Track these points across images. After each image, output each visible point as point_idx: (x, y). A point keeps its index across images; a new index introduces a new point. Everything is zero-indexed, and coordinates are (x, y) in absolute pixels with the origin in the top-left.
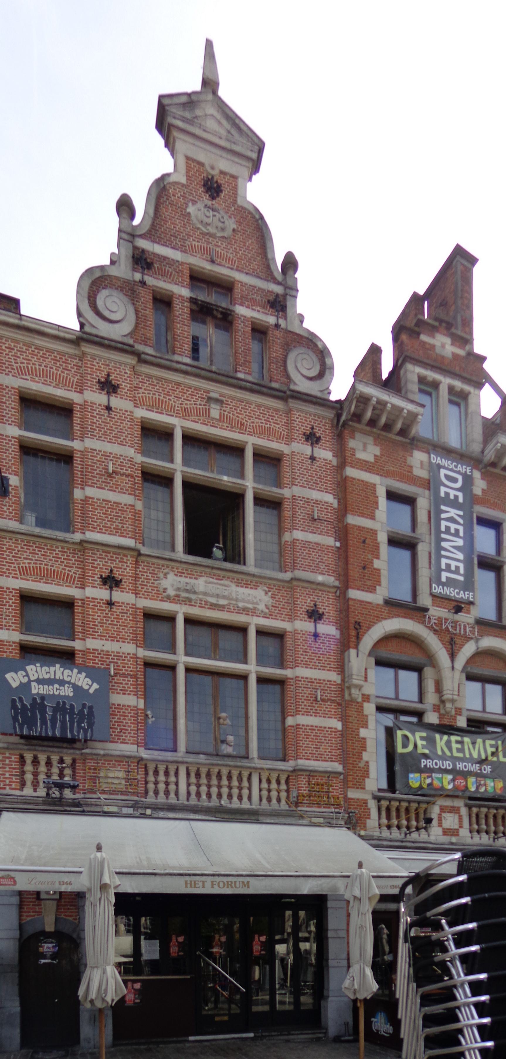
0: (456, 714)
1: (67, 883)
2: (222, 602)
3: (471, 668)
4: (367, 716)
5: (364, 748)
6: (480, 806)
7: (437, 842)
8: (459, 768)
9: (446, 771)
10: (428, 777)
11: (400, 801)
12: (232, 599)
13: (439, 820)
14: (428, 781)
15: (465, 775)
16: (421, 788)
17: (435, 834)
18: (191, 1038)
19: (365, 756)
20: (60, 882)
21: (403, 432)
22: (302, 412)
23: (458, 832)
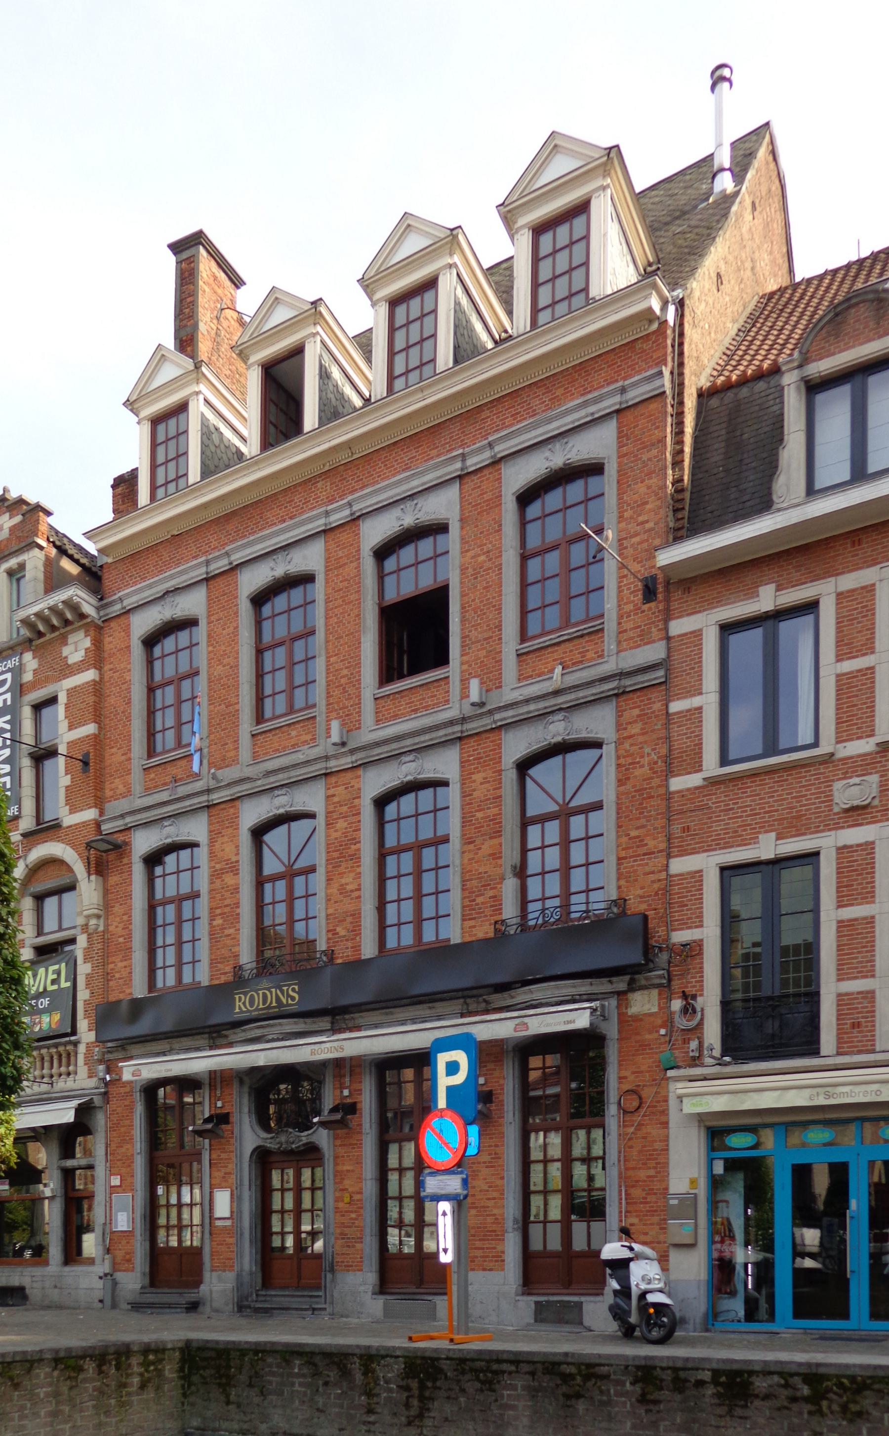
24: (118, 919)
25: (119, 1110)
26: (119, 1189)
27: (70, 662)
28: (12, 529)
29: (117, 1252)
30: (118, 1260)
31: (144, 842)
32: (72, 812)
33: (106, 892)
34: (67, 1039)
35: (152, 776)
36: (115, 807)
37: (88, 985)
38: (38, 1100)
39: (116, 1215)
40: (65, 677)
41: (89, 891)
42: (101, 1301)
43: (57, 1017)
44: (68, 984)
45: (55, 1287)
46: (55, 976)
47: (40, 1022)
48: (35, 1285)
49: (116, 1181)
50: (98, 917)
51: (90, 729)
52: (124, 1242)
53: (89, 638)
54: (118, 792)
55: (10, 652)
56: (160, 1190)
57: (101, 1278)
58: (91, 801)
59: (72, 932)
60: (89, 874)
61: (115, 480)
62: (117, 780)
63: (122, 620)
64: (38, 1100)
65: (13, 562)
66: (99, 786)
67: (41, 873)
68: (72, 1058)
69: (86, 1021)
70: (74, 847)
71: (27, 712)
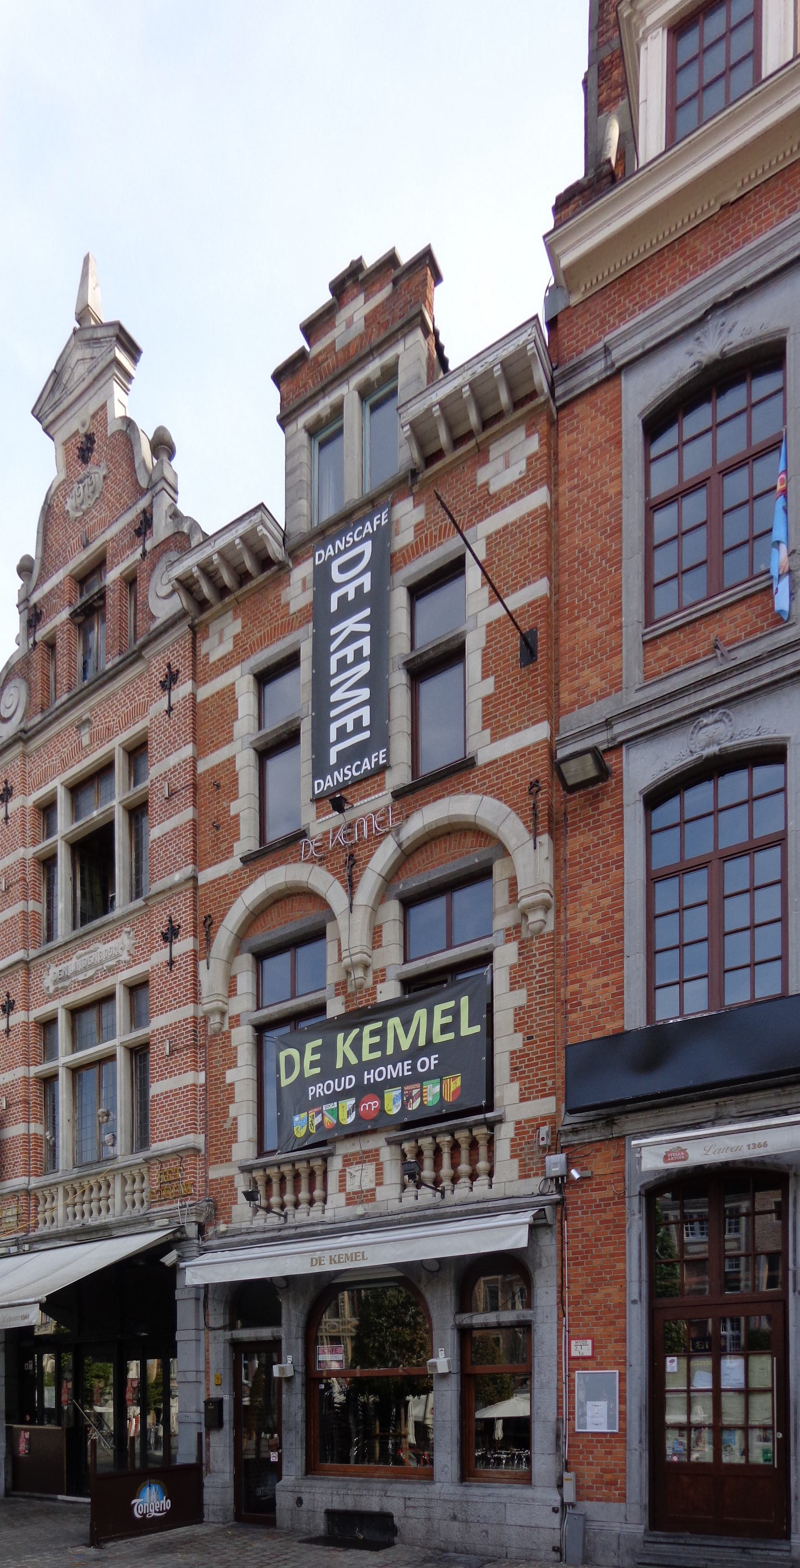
0: (375, 983)
1: (760, 1146)
2: (90, 973)
3: (404, 884)
4: (236, 1048)
5: (231, 1099)
6: (415, 1138)
7: (337, 1219)
8: (369, 1079)
9: (345, 1094)
10: (317, 1114)
11: (278, 1165)
12: (97, 965)
13: (340, 1181)
14: (317, 1120)
15: (378, 1090)
16: (308, 1134)
17: (336, 1207)
18: (60, 1497)
19: (233, 1110)
20: (749, 1146)
21: (265, 562)
22: (159, 654)
23: (374, 1195)
24: (589, 906)
25: (590, 1229)
26: (590, 1362)
27: (493, 489)
28: (369, 319)
29: (584, 1468)
30: (587, 1481)
31: (643, 768)
32: (494, 738)
33: (559, 864)
34: (481, 1117)
35: (664, 650)
36: (571, 723)
37: (518, 1026)
38: (273, 1239)
39: (583, 1405)
40: (484, 516)
41: (530, 863)
42: (556, 1549)
43: (455, 1083)
44: (477, 1029)
45: (454, 1518)
46: (449, 1019)
47: (421, 1094)
48: (410, 1512)
49: (582, 1348)
50: (546, 906)
51: (540, 588)
52: (600, 1451)
53: (536, 438)
54: (588, 691)
55: (368, 509)
56: (672, 1365)
57: (555, 1510)
58: (541, 709)
59: (485, 943)
60: (535, 834)
61: (558, 198)
62: (587, 672)
63: (604, 396)
64: (273, 1239)
65: (372, 369)
66: (553, 688)
67: (419, 858)
68: (483, 1150)
69: (516, 1086)
70: (500, 794)
71: (400, 597)
